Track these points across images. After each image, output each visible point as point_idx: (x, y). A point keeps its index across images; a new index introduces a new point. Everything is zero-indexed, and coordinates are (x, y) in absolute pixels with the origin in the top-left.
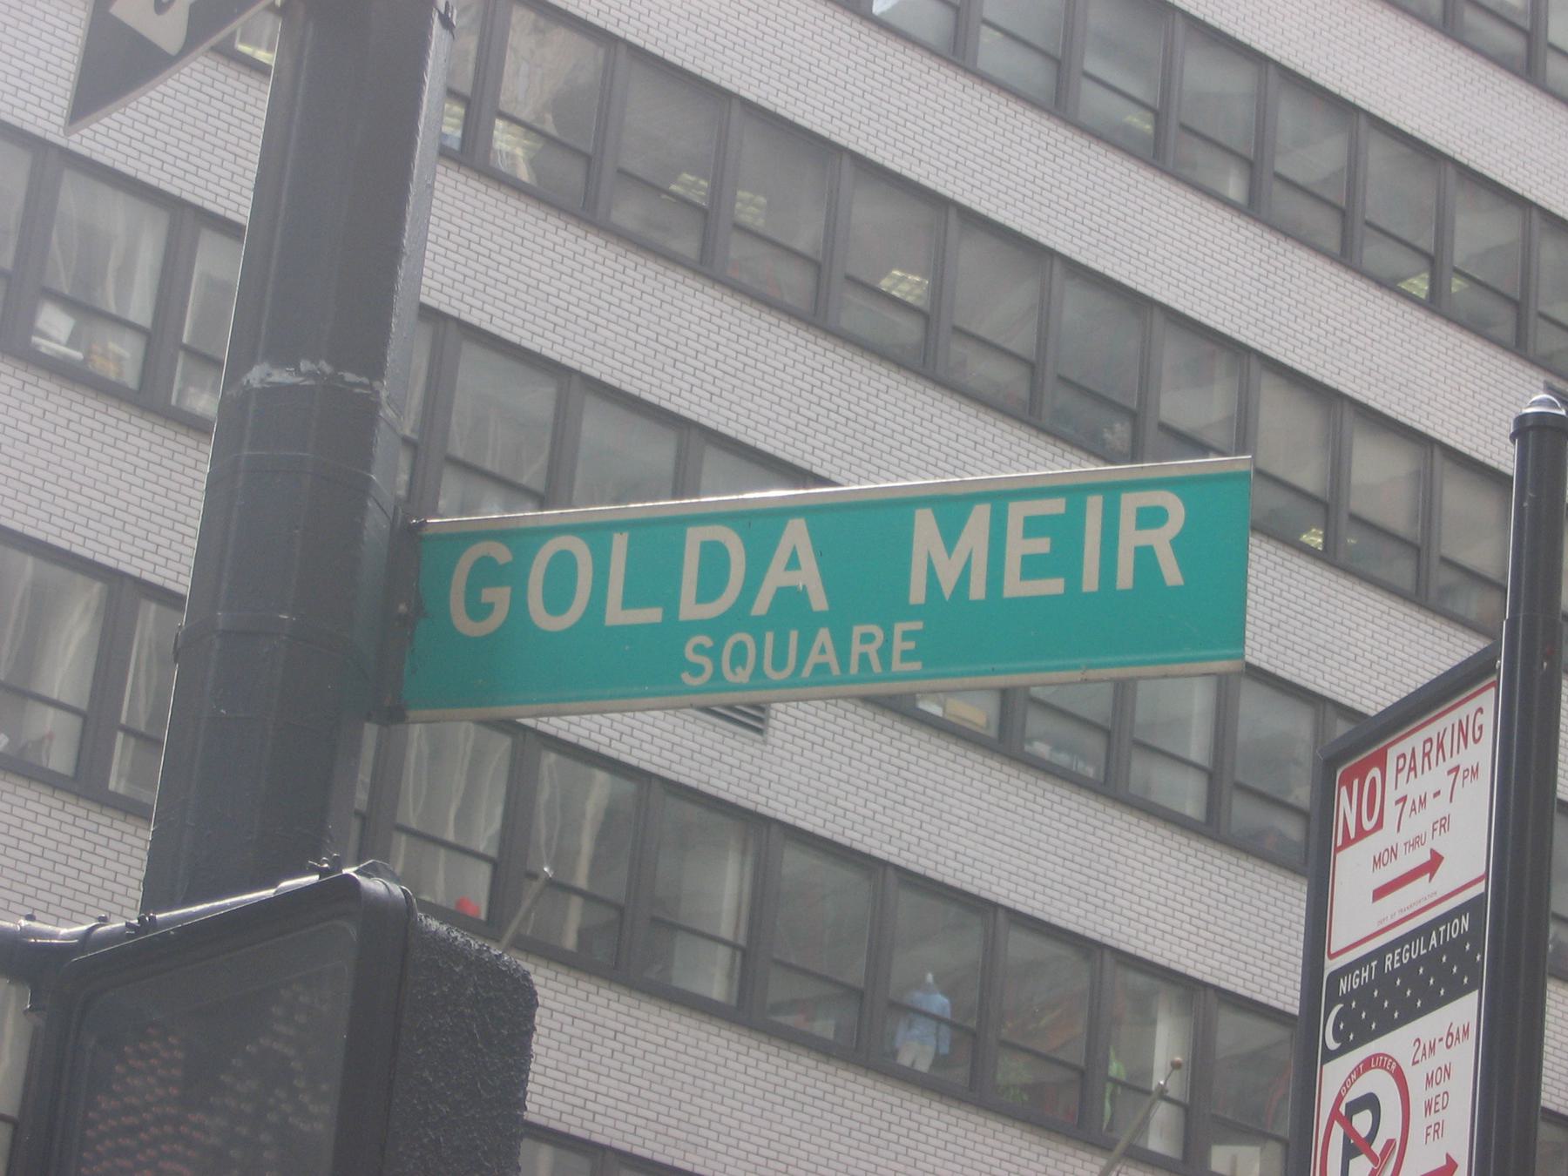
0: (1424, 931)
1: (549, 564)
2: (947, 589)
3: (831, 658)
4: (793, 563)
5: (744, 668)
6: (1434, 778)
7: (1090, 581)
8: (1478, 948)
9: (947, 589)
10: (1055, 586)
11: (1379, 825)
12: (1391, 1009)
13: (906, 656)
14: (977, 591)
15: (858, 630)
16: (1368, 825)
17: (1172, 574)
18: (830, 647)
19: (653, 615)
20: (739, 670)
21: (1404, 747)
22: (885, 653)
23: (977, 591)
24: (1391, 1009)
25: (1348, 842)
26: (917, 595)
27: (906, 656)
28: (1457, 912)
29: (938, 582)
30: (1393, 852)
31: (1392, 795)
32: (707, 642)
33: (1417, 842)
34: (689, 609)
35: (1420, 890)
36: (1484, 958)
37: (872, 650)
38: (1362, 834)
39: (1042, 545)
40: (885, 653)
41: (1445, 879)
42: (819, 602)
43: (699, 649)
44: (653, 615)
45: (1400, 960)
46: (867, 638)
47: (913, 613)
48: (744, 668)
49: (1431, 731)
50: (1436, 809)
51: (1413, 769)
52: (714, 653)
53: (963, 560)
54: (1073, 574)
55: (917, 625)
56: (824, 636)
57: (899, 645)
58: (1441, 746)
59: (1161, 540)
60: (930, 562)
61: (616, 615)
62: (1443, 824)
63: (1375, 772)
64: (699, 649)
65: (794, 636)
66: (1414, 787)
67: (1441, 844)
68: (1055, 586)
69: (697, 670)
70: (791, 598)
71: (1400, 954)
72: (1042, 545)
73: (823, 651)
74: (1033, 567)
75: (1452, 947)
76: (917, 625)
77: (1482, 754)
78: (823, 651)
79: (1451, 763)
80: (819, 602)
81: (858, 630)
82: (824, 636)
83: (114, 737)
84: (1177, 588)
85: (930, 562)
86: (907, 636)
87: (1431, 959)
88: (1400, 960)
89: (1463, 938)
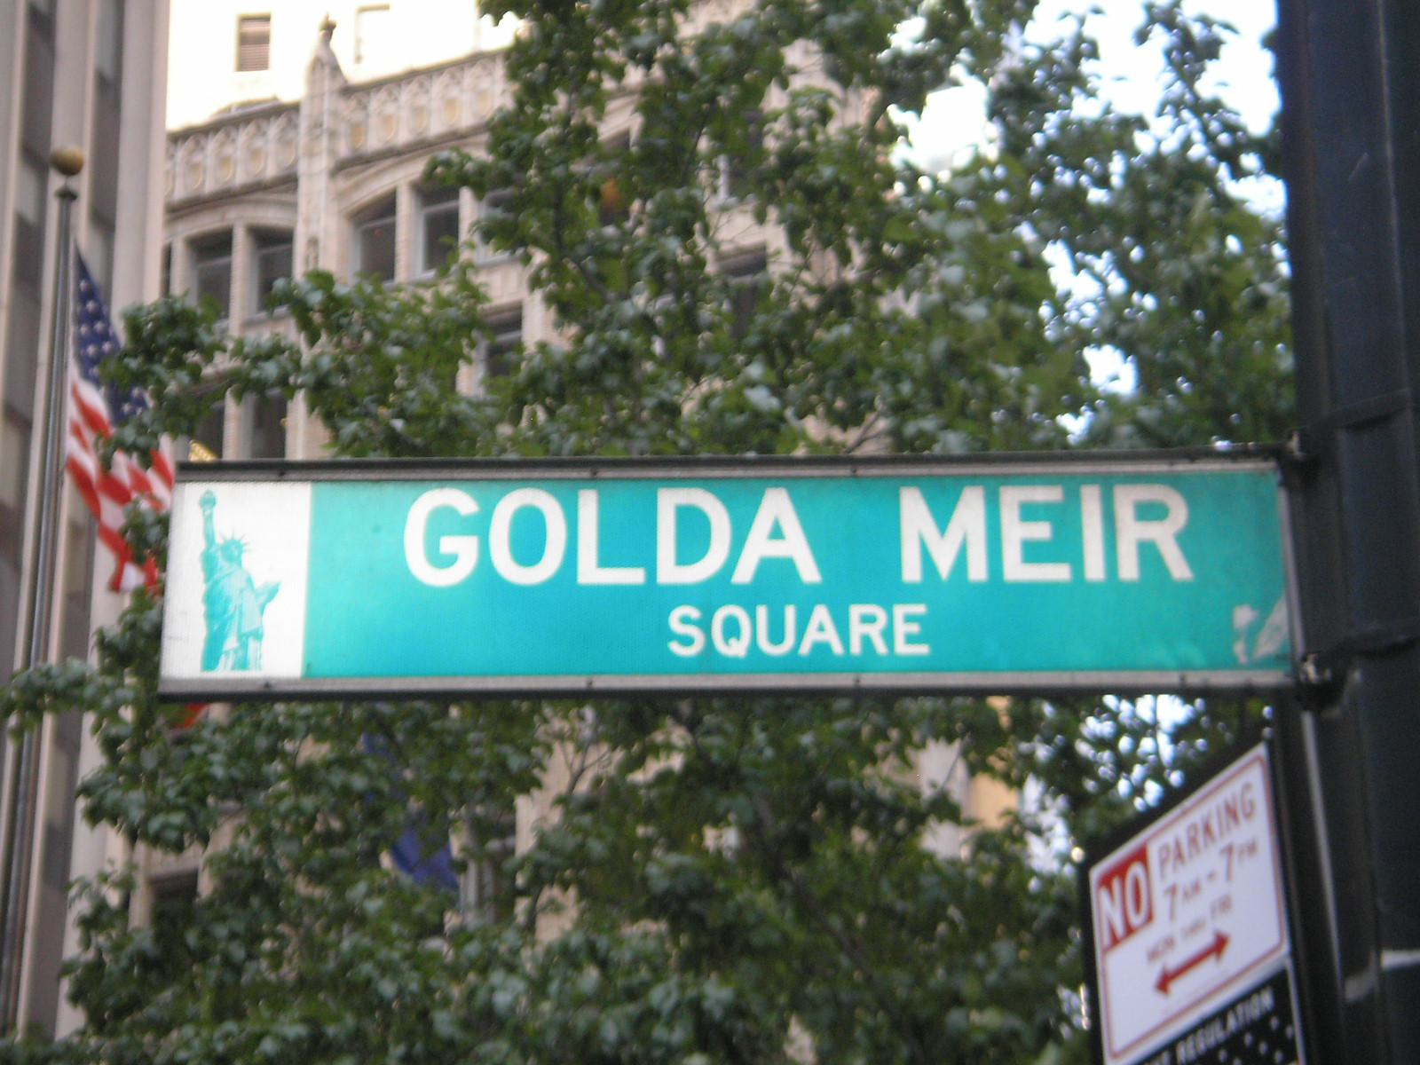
0: (1221, 1015)
4: (777, 533)
5: (738, 639)
6: (1209, 860)
7: (1095, 569)
8: (1286, 1019)
10: (1058, 572)
11: (1150, 917)
13: (910, 639)
14: (978, 571)
15: (856, 611)
16: (1135, 920)
17: (1179, 568)
19: (635, 576)
20: (733, 641)
21: (1168, 838)
22: (888, 635)
23: (978, 571)
25: (1115, 941)
26: (911, 571)
27: (910, 639)
28: (1257, 990)
30: (1169, 943)
31: (1159, 888)
32: (694, 613)
33: (1195, 928)
34: (669, 572)
35: (1208, 973)
36: (1295, 1031)
37: (874, 631)
38: (1130, 930)
39: (1041, 531)
40: (888, 635)
41: (1234, 958)
42: (809, 572)
43: (685, 620)
44: (635, 576)
46: (868, 619)
47: (911, 594)
48: (738, 639)
49: (1196, 817)
50: (1211, 893)
51: (1179, 856)
52: (705, 625)
53: (959, 539)
54: (1077, 563)
55: (920, 609)
56: (821, 614)
57: (901, 629)
58: (1207, 829)
61: (590, 573)
62: (1225, 904)
63: (1136, 870)
64: (685, 620)
66: (1183, 876)
67: (1225, 924)
68: (1058, 572)
69: (687, 641)
72: (1041, 531)
73: (821, 628)
74: (1032, 552)
75: (1258, 1027)
76: (920, 609)
77: (1258, 829)
78: (821, 628)
79: (1222, 843)
80: (809, 572)
81: (856, 611)
82: (821, 614)
86: (909, 619)
89: (1265, 1017)
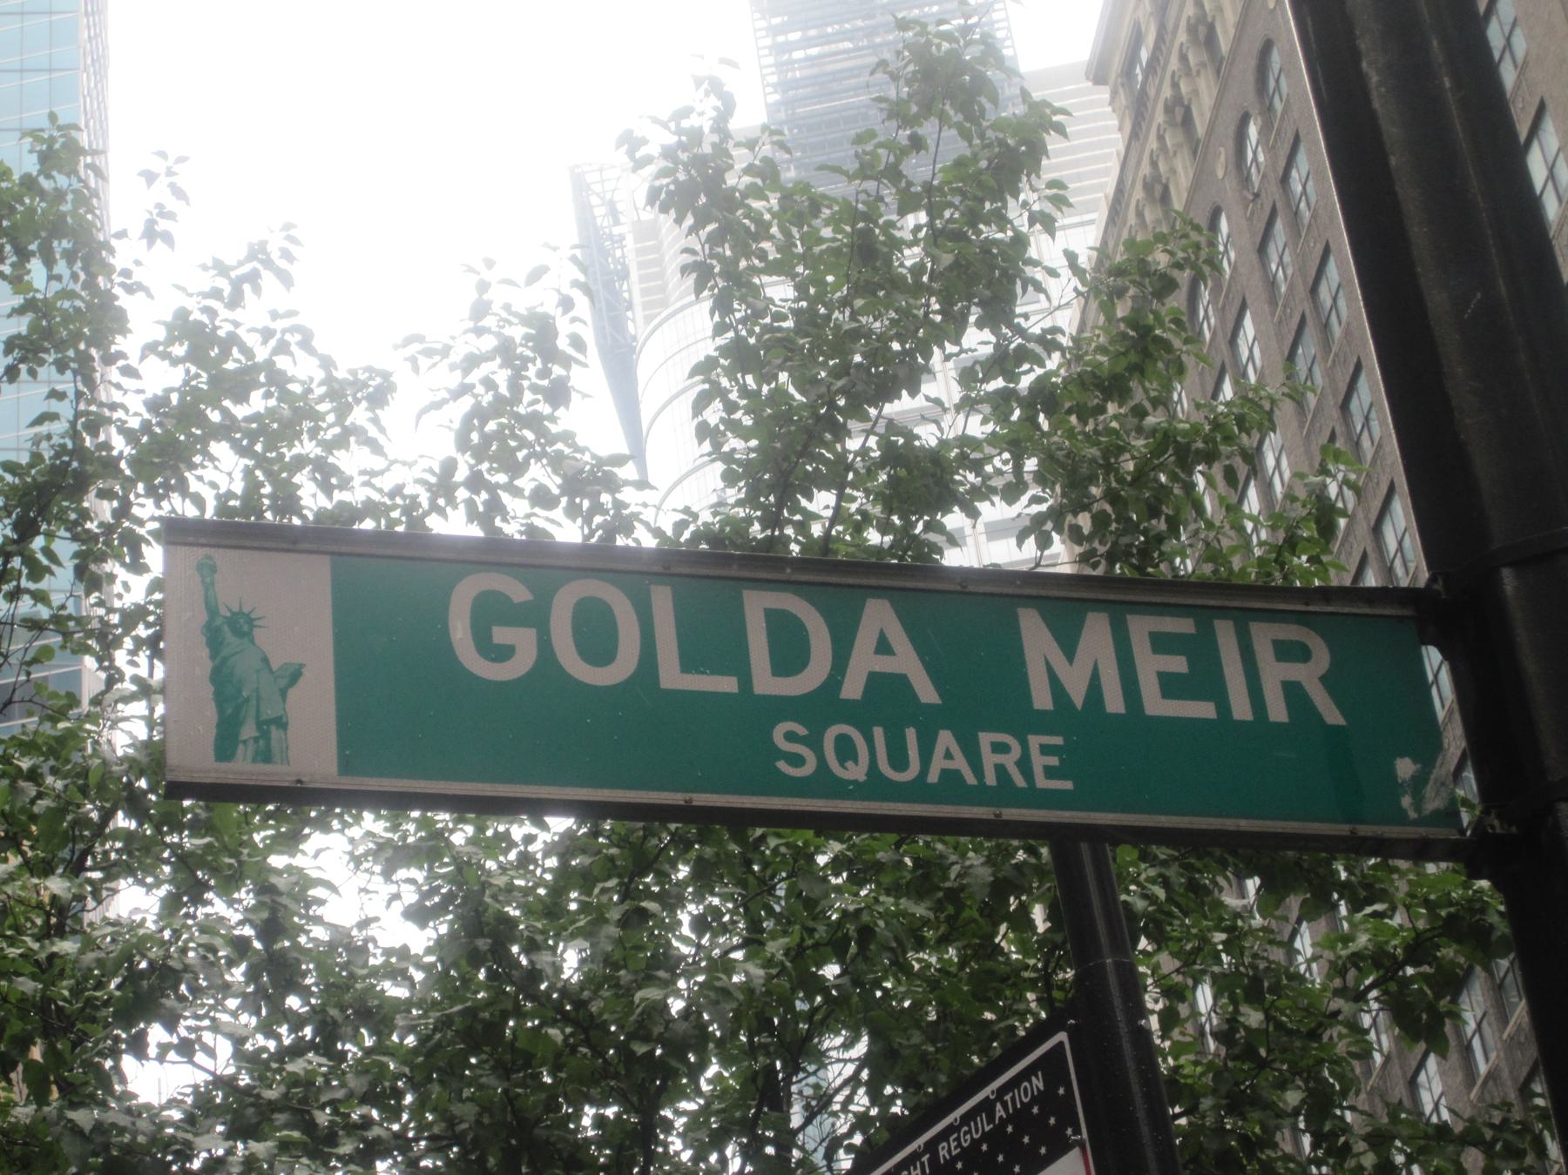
1: (795, 617)
2: (1078, 699)
3: (960, 763)
5: (856, 762)
9: (1078, 699)
12: (1035, 1145)
13: (1050, 772)
18: (955, 749)
20: (849, 764)
23: (1114, 703)
24: (1035, 1145)
29: (1063, 690)
34: (766, 683)
37: (1010, 761)
42: (927, 693)
43: (790, 737)
45: (959, 1145)
48: (856, 762)
59: (1309, 675)
60: (1047, 663)
61: (671, 676)
64: (790, 737)
65: (911, 735)
69: (797, 760)
70: (888, 689)
71: (958, 1139)
72: (1178, 664)
74: (1171, 686)
80: (927, 693)
82: (945, 739)
83: (778, 770)
84: (1043, 713)
85: (1047, 663)
87: (995, 1137)
88: (959, 1145)
